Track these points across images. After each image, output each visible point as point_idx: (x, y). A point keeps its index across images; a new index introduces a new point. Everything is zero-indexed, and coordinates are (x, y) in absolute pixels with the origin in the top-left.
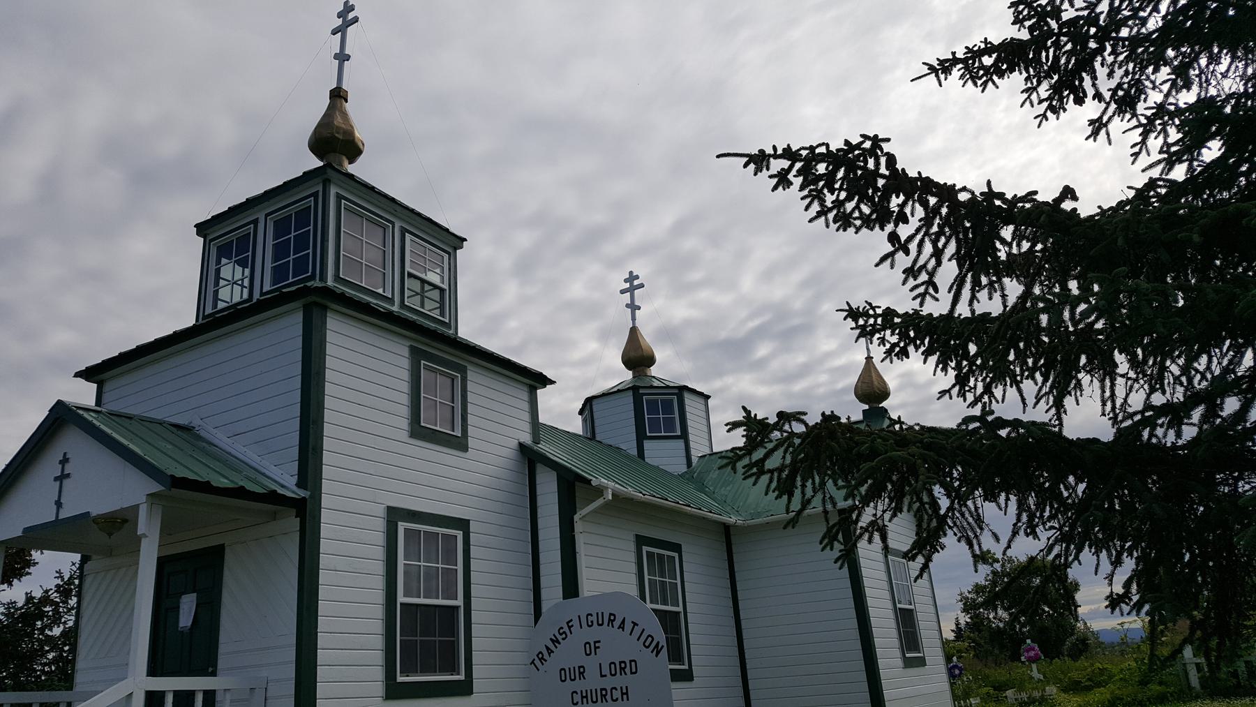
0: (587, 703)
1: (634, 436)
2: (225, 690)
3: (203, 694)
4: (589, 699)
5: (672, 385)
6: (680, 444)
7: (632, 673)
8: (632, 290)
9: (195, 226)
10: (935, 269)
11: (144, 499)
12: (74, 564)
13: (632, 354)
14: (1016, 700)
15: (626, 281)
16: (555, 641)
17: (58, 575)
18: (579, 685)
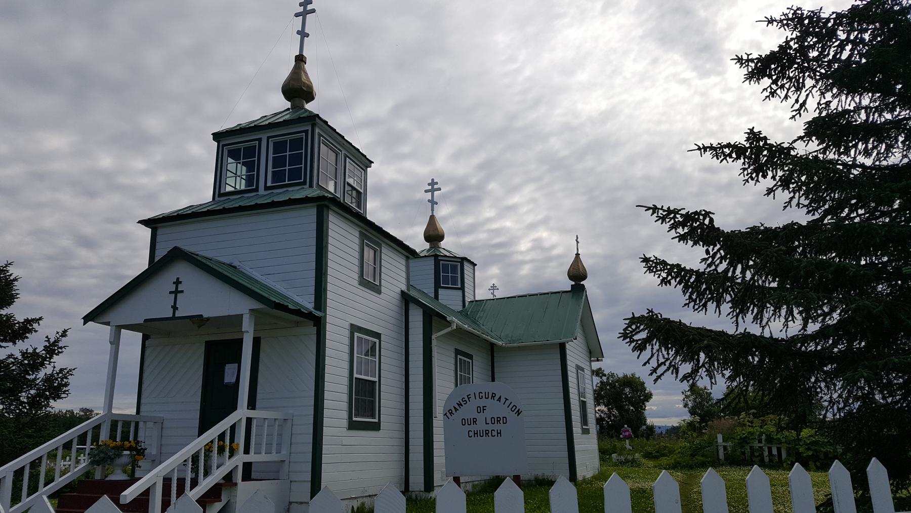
0: (477, 436)
1: (433, 285)
2: (265, 419)
3: (123, 423)
4: (479, 435)
5: (458, 256)
6: (460, 293)
7: (504, 423)
8: (432, 191)
9: (212, 134)
10: (718, 265)
11: (248, 312)
12: (58, 333)
13: (431, 233)
14: (617, 460)
15: (429, 184)
16: (460, 405)
17: (47, 339)
18: (473, 427)
